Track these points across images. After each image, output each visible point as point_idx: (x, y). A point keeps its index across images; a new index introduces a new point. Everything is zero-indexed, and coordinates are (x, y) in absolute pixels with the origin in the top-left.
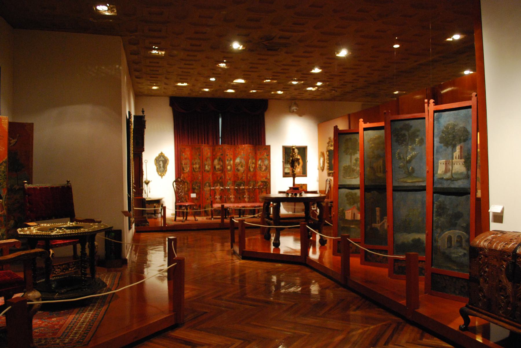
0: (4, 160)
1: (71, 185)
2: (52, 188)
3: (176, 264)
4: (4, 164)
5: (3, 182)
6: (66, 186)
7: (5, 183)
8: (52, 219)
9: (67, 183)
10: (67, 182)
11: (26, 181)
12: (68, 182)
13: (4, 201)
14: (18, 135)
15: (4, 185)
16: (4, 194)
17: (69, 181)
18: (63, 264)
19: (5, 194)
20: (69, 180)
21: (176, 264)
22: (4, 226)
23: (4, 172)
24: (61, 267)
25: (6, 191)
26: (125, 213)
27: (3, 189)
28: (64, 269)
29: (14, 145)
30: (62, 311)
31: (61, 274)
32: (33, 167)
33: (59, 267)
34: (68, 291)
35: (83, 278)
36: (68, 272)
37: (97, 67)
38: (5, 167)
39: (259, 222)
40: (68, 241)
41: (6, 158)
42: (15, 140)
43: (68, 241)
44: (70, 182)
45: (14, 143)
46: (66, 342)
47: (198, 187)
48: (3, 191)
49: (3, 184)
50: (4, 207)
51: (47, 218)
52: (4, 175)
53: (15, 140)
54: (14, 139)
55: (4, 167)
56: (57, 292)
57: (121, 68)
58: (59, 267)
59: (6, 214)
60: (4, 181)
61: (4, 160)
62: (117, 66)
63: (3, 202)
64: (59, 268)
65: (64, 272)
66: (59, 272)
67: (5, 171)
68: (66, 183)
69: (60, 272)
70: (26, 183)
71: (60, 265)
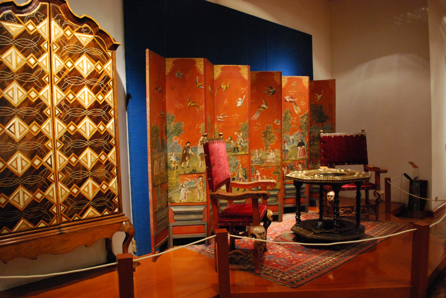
0: (306, 113)
1: (365, 134)
2: (346, 137)
3: (416, 229)
4: (306, 116)
5: (305, 132)
6: (360, 135)
7: (307, 132)
8: (345, 165)
9: (362, 133)
10: (362, 131)
11: (322, 131)
12: (363, 131)
13: (306, 147)
14: (323, 91)
15: (306, 133)
16: (306, 141)
17: (364, 131)
18: (347, 207)
19: (307, 142)
20: (363, 129)
21: (416, 229)
22: (306, 168)
23: (305, 123)
24: (345, 210)
25: (308, 139)
26: (294, 169)
27: (305, 137)
28: (347, 211)
29: (320, 99)
30: (314, 249)
31: (343, 215)
32: (336, 118)
33: (343, 209)
34: (321, 233)
35: (335, 224)
36: (352, 215)
37: (402, 15)
38: (306, 119)
39: (368, 198)
40: (352, 187)
41: (307, 111)
42: (321, 96)
43: (352, 187)
44: (365, 131)
45: (320, 98)
46: (283, 279)
47: (172, 147)
48: (305, 139)
49: (305, 133)
50: (306, 153)
51: (340, 164)
52: (306, 126)
53: (321, 96)
54: (320, 95)
55: (305, 119)
56: (313, 232)
57: (427, 9)
58: (343, 209)
59: (307, 157)
60: (306, 131)
61: (305, 113)
62: (423, 9)
63: (305, 148)
64: (342, 210)
65: (348, 214)
66: (342, 213)
67: (306, 122)
68: (361, 132)
69: (343, 213)
70: (322, 132)
71: (344, 207)
